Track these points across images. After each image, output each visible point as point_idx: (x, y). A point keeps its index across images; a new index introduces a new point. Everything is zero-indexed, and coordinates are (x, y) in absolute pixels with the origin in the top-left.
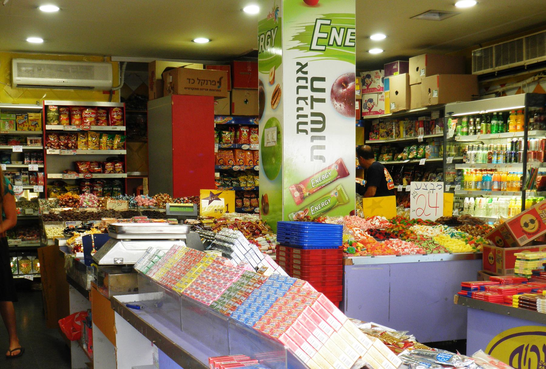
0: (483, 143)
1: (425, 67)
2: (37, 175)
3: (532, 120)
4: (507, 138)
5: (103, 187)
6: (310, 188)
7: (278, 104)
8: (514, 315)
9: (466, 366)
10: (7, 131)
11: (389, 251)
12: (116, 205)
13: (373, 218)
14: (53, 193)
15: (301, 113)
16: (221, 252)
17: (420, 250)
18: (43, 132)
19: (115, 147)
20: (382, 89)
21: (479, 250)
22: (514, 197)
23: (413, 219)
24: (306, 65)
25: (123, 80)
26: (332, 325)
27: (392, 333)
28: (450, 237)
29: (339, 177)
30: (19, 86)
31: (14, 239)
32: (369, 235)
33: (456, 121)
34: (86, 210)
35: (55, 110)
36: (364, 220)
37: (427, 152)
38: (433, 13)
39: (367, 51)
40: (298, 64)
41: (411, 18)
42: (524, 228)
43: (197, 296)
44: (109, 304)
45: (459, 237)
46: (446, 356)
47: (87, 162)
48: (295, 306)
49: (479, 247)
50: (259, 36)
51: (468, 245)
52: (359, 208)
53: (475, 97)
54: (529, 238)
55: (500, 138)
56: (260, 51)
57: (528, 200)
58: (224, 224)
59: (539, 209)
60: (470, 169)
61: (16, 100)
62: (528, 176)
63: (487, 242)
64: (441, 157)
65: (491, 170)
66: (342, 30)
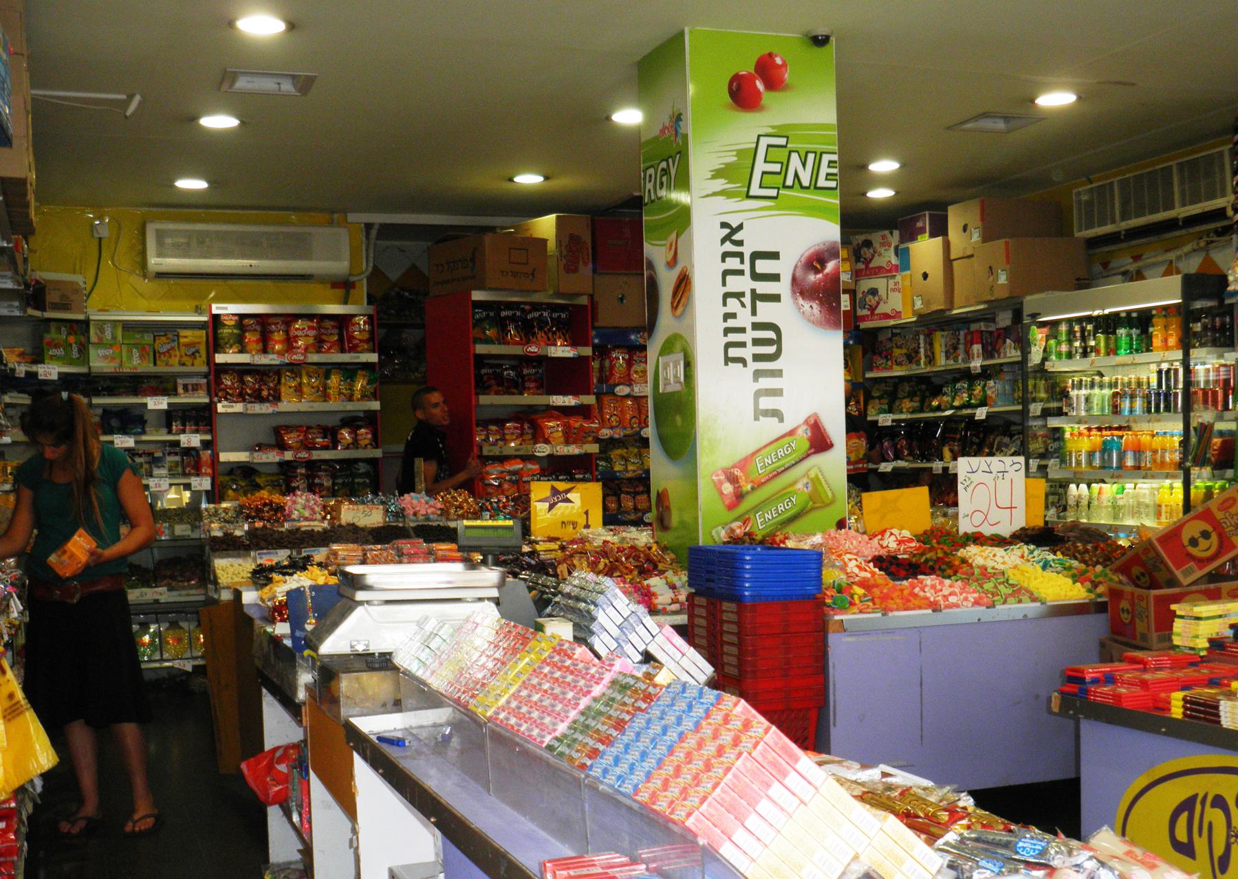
0: (1101, 375)
1: (979, 224)
2: (198, 456)
3: (1197, 327)
4: (1149, 363)
5: (334, 476)
6: (754, 476)
7: (685, 306)
8: (1176, 730)
9: (1077, 865)
10: (136, 368)
11: (917, 602)
12: (360, 515)
13: (883, 532)
14: (230, 492)
15: (731, 323)
16: (571, 620)
17: (980, 598)
18: (210, 368)
19: (358, 395)
20: (896, 268)
21: (1100, 595)
22: (1168, 482)
23: (966, 534)
24: (740, 227)
25: (371, 259)
26: (796, 791)
27: (925, 789)
28: (1040, 569)
29: (812, 451)
30: (161, 275)
31: (152, 587)
32: (876, 570)
33: (1045, 330)
34: (298, 524)
35: (233, 323)
36: (866, 537)
37: (989, 392)
38: (991, 117)
39: (864, 194)
40: (724, 225)
41: (949, 128)
42: (1191, 549)
43: (520, 725)
44: (342, 733)
45: (1060, 569)
46: (1035, 845)
47: (302, 426)
48: (720, 751)
49: (1101, 589)
50: (645, 171)
51: (1078, 585)
52: (854, 514)
53: (1082, 282)
54: (1200, 568)
55: (1136, 364)
56: (646, 200)
57: (1196, 487)
58: (581, 553)
59: (1219, 510)
60: (1076, 426)
61: (154, 304)
62: (1194, 440)
63: (1115, 578)
64: (1019, 404)
65: (1120, 428)
66: (811, 157)
